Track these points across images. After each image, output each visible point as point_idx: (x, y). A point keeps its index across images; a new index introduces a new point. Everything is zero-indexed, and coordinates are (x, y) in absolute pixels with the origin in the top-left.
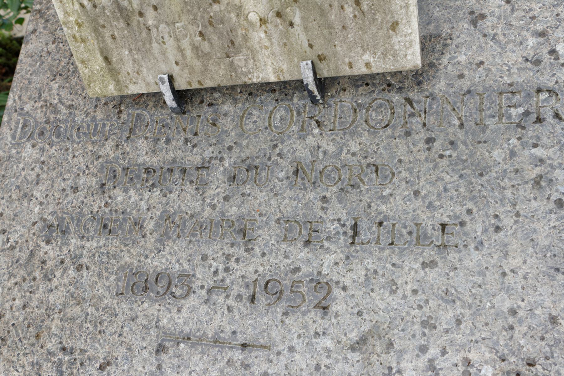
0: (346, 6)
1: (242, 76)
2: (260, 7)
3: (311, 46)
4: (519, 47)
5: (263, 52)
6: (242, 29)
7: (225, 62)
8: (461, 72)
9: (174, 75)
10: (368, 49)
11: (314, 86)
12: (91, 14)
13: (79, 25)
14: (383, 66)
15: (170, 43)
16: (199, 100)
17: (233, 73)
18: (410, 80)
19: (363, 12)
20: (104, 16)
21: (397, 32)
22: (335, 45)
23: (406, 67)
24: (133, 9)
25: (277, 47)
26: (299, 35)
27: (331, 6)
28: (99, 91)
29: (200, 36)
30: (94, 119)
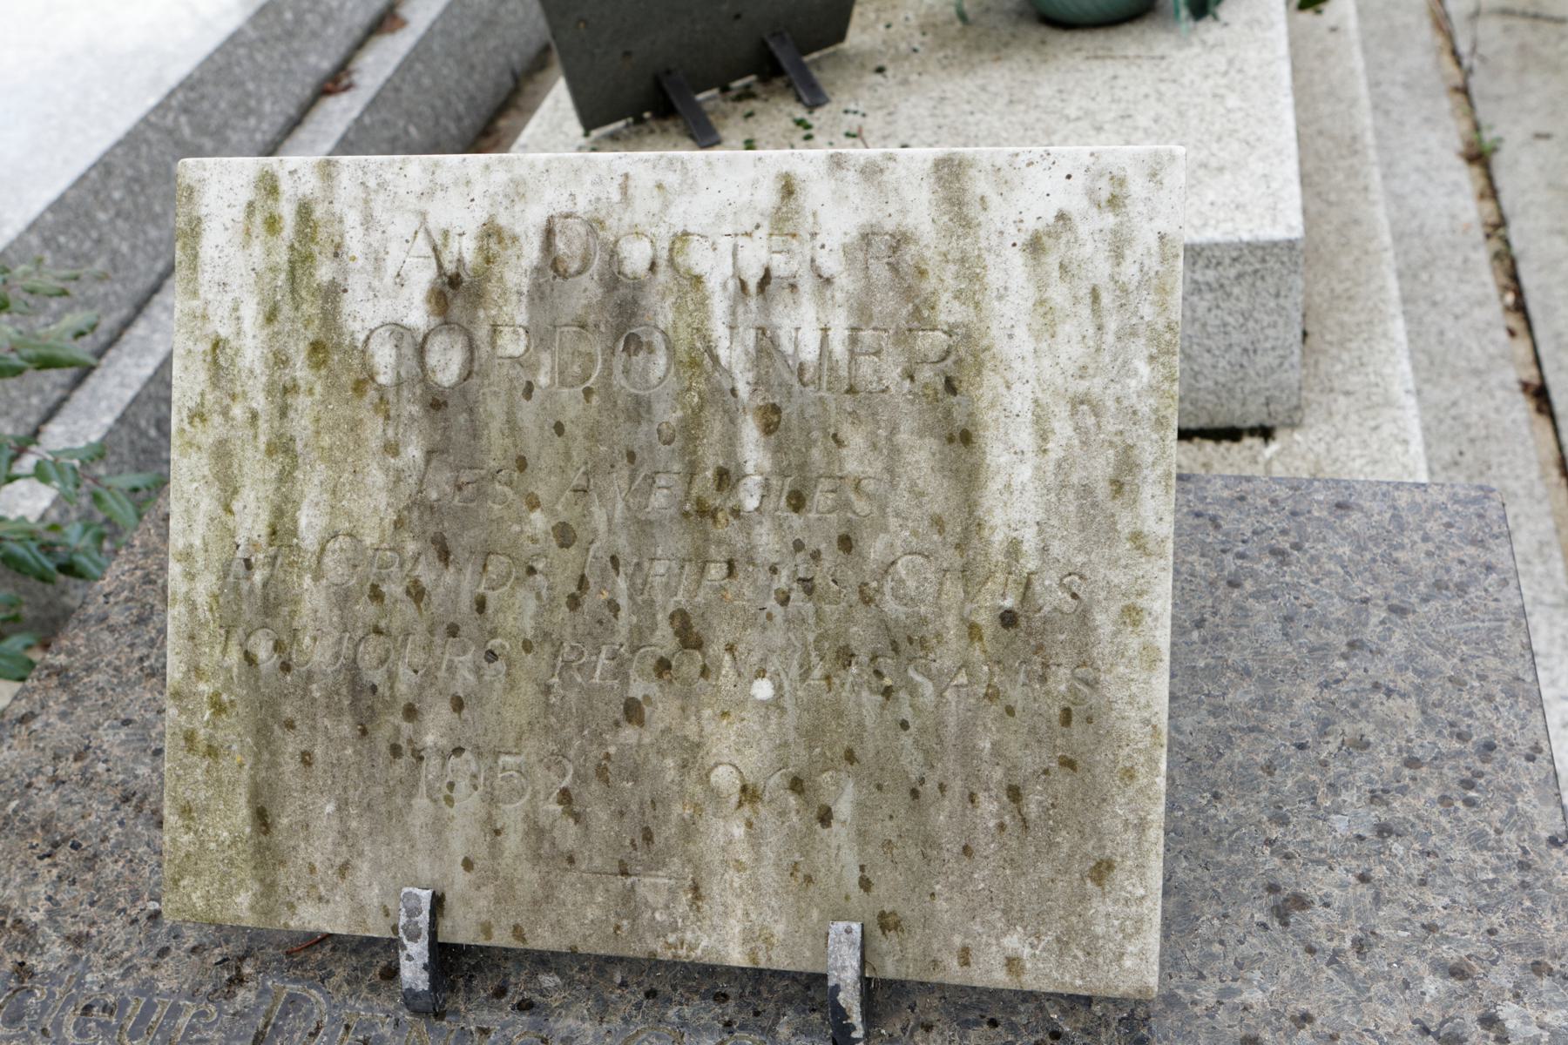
0: (982, 797)
1: (648, 935)
2: (752, 755)
3: (865, 884)
4: (1403, 993)
5: (727, 876)
6: (684, 805)
7: (611, 887)
8: (1252, 1033)
9: (448, 897)
10: (1022, 919)
11: (857, 996)
12: (267, 685)
13: (218, 707)
14: (1055, 974)
15: (468, 802)
16: (492, 985)
17: (625, 922)
18: (1112, 1030)
19: (1024, 820)
20: (302, 698)
21: (1107, 888)
22: (933, 894)
23: (1117, 988)
24: (392, 696)
25: (771, 870)
26: (839, 848)
27: (942, 787)
28: (200, 904)
29: (560, 803)
30: (147, 988)
